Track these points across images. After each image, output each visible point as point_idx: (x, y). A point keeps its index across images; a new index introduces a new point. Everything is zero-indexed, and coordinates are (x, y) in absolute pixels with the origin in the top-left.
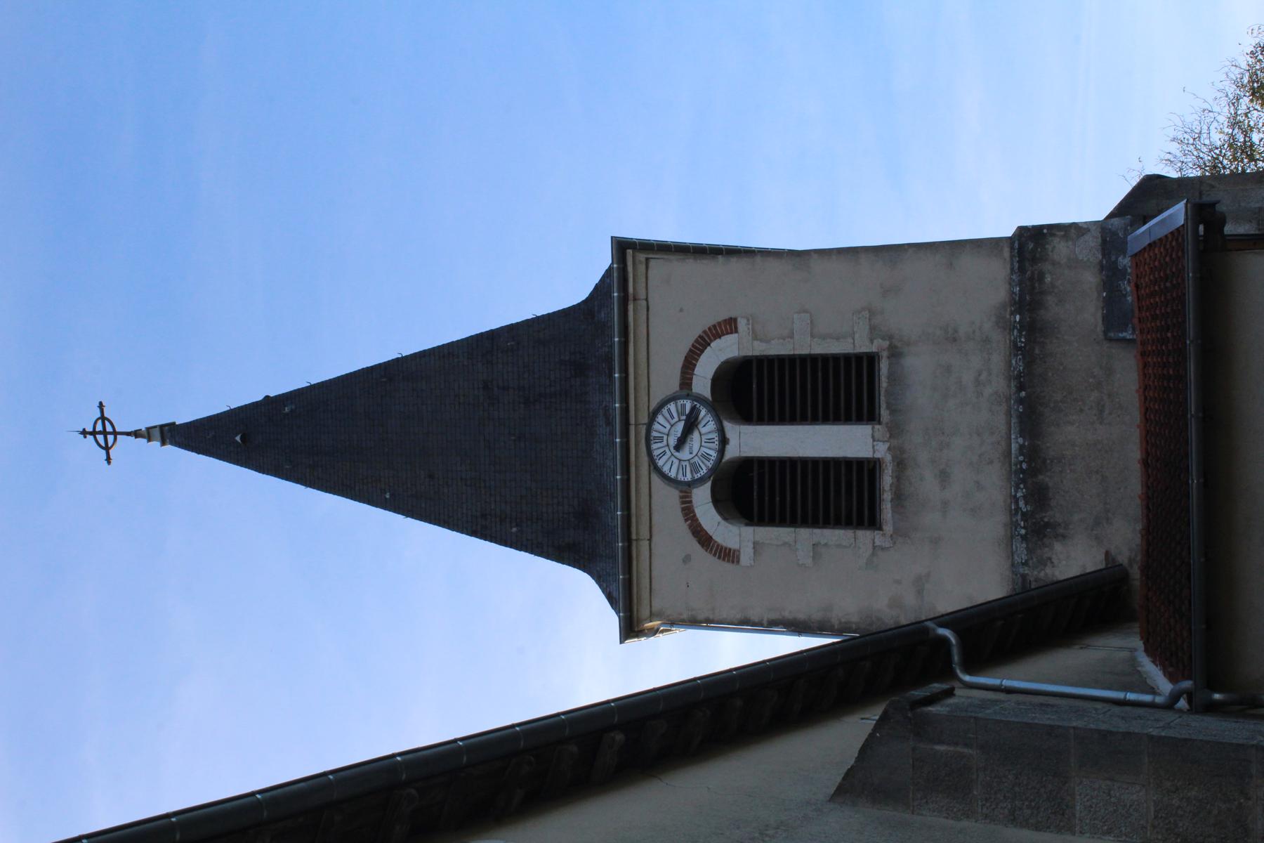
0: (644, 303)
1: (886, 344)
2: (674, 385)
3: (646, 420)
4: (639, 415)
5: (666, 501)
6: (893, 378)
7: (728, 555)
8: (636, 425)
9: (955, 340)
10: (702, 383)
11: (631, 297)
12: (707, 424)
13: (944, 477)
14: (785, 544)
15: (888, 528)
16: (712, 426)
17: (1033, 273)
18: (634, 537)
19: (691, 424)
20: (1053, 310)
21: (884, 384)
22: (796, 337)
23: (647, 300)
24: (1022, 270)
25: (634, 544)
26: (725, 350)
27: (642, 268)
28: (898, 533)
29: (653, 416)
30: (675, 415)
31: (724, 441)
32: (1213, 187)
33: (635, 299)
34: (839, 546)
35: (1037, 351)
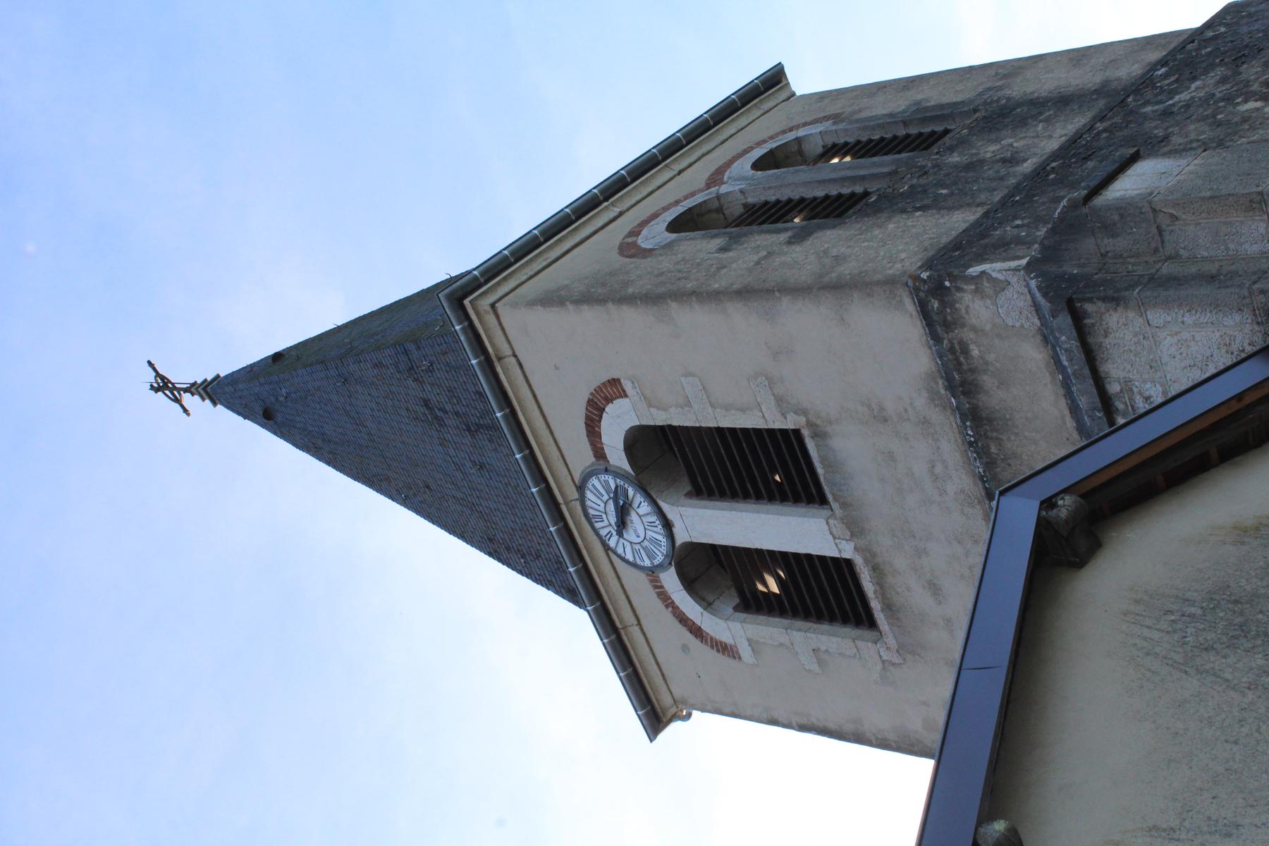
0: (513, 360)
1: (802, 420)
2: (588, 458)
3: (576, 495)
4: (565, 491)
5: (637, 584)
6: (823, 460)
7: (724, 649)
8: (567, 504)
9: (886, 420)
10: (617, 457)
11: (494, 358)
12: (641, 507)
13: (934, 588)
14: (781, 645)
15: (890, 640)
16: (645, 508)
17: (950, 341)
18: (618, 625)
19: (623, 512)
20: (994, 397)
21: (820, 471)
22: (695, 406)
23: (515, 356)
24: (935, 337)
25: (622, 632)
26: (617, 424)
27: (491, 319)
28: (901, 649)
29: (581, 488)
30: (603, 492)
31: (668, 525)
32: (1174, 218)
33: (500, 359)
34: (842, 654)
35: (993, 449)
